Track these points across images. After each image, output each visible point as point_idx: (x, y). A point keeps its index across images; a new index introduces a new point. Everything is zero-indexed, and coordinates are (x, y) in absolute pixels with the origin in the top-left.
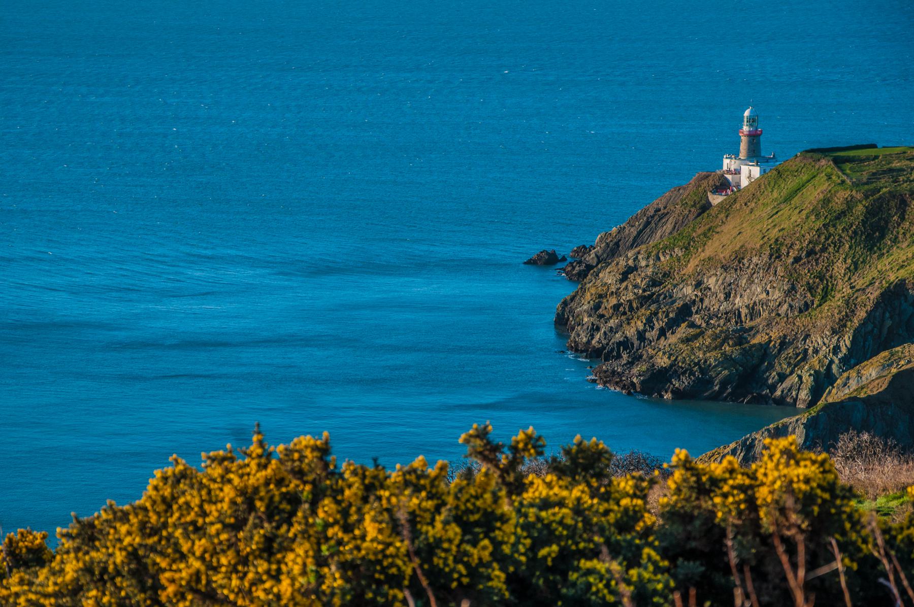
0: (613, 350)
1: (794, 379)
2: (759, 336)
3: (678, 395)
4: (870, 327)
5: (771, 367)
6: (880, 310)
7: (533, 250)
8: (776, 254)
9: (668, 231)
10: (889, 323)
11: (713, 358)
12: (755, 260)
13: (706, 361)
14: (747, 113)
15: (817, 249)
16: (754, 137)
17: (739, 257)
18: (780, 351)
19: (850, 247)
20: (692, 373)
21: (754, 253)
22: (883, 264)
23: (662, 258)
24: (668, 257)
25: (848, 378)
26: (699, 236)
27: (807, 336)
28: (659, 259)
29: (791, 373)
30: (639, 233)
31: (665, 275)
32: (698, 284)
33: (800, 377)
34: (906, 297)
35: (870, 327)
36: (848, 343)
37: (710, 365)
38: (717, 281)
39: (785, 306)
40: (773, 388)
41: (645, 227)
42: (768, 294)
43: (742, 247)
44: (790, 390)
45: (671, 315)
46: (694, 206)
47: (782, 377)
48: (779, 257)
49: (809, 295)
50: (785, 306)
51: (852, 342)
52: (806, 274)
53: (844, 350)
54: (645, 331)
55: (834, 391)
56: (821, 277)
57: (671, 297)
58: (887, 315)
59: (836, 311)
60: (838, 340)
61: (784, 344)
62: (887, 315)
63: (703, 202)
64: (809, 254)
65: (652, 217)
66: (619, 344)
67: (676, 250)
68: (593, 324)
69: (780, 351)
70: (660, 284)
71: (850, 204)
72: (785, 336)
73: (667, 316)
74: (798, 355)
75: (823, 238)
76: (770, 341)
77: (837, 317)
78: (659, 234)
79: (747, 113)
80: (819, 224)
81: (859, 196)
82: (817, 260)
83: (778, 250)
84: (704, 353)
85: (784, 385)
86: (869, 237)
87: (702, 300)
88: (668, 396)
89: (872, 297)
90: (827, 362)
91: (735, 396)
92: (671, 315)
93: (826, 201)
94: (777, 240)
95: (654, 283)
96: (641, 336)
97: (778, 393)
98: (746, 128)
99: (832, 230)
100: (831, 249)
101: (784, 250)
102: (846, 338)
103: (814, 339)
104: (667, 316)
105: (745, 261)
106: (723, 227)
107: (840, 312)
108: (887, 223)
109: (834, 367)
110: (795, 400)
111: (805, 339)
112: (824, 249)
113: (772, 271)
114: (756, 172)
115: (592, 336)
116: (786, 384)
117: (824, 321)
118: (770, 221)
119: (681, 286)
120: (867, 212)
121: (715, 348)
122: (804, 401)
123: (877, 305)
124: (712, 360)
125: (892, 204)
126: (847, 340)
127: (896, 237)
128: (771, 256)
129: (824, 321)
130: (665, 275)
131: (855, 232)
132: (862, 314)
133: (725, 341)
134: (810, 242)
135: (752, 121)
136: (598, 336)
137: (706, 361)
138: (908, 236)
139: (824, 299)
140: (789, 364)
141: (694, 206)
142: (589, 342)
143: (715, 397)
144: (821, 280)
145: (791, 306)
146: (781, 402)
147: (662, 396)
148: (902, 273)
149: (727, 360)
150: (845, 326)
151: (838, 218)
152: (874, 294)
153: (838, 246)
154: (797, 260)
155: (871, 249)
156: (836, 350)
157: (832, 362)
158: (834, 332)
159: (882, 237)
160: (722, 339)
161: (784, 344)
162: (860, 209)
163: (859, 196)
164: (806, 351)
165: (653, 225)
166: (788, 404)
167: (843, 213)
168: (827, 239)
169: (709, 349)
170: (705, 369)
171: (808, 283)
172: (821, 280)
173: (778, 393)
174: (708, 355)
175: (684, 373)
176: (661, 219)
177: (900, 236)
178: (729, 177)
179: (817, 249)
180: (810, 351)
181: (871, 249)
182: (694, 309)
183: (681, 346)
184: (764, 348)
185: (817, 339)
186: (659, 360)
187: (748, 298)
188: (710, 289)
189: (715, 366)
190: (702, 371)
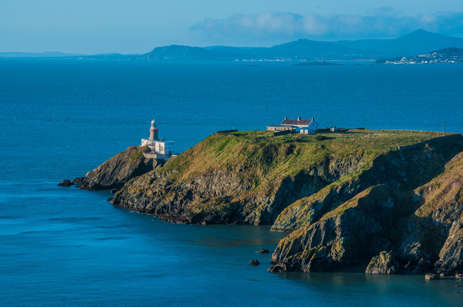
0: (160, 209)
1: (253, 214)
2: (234, 199)
3: (208, 223)
4: (280, 193)
5: (242, 210)
6: (283, 187)
7: (61, 181)
8: (230, 169)
9: (128, 169)
10: (286, 191)
11: (219, 208)
12: (219, 172)
13: (216, 210)
14: (152, 122)
15: (248, 166)
16: (155, 131)
17: (211, 171)
18: (244, 204)
19: (261, 165)
20: (212, 214)
21: (218, 169)
22: (277, 170)
23: (168, 174)
24: (170, 174)
25: (287, 210)
26: (183, 165)
27: (255, 198)
28: (166, 175)
29: (251, 212)
30: (114, 170)
31: (173, 180)
32: (193, 183)
33: (255, 213)
34: (291, 182)
35: (280, 193)
36: (273, 199)
37: (218, 211)
38: (202, 181)
39: (240, 188)
40: (244, 218)
41: (116, 168)
42: (230, 184)
43: (210, 167)
44: (251, 218)
45: (185, 195)
46: (138, 158)
47: (248, 214)
48: (231, 170)
49: (249, 183)
50: (240, 188)
51: (275, 199)
52: (246, 175)
53: (272, 202)
54: (173, 201)
55: (282, 216)
56: (253, 177)
57: (180, 188)
58: (286, 188)
59: (266, 188)
60: (269, 199)
61: (246, 202)
62: (286, 188)
63: (142, 157)
64: (246, 168)
65: (119, 164)
66: (163, 207)
67: (174, 171)
68: (146, 201)
69: (244, 204)
70: (172, 184)
71: (256, 150)
72: (246, 199)
73: (183, 195)
74: (253, 205)
75: (249, 162)
76: (240, 201)
77: (267, 190)
78: (123, 170)
79: (152, 122)
80: (246, 157)
81: (258, 146)
82: (249, 170)
83: (230, 167)
84: (212, 206)
85: (248, 217)
86: (267, 161)
87: (196, 188)
88: (204, 223)
89: (279, 182)
90: (265, 207)
91: (229, 222)
92: (185, 195)
93: (245, 149)
94: (227, 164)
95: (169, 184)
96: (172, 203)
97: (246, 220)
98: (152, 128)
99: (252, 159)
100: (253, 166)
101: (233, 167)
102: (272, 197)
103: (258, 199)
104: (183, 195)
105: (214, 172)
106: (193, 161)
107: (268, 188)
108: (272, 156)
109: (268, 209)
110: (253, 222)
111: (254, 199)
112: (251, 166)
113: (230, 175)
114: (143, 145)
115: (146, 206)
116: (250, 216)
117: (261, 192)
118: (219, 157)
119: (184, 184)
120: (264, 152)
121: (218, 205)
122: (257, 222)
123: (282, 185)
124: (219, 209)
125: (272, 149)
126: (273, 198)
127: (277, 161)
128: (228, 170)
129: (261, 192)
130: (173, 180)
131: (261, 159)
132: (276, 189)
133: (221, 201)
134: (244, 164)
135: (155, 125)
136: (149, 205)
137: (216, 210)
138: (281, 160)
139: (257, 185)
140: (250, 209)
141: (138, 158)
142: (145, 208)
143: (222, 223)
144: (253, 177)
145: (242, 188)
146: (247, 223)
147: (201, 224)
148: (287, 173)
149: (225, 209)
150: (271, 193)
151: (253, 154)
152: (279, 181)
153: (256, 165)
154: (241, 170)
155: (269, 165)
156: (269, 202)
157: (267, 207)
158: (267, 196)
159: (271, 161)
160: (219, 201)
161: (246, 202)
162: (260, 151)
163: (258, 146)
164: (256, 203)
165: (119, 166)
166: (250, 224)
167: (253, 153)
168: (251, 162)
169: (215, 205)
170: (217, 212)
171: (248, 179)
172: (253, 177)
173: (246, 220)
174: (216, 207)
175: (208, 214)
176: (123, 164)
177: (278, 161)
178: (150, 147)
179: (248, 166)
180: (258, 203)
181: (269, 165)
182: (193, 192)
183: (203, 204)
184: (238, 203)
185: (259, 199)
186: (194, 211)
187: (219, 186)
188: (198, 184)
189: (221, 211)
190: (215, 213)
